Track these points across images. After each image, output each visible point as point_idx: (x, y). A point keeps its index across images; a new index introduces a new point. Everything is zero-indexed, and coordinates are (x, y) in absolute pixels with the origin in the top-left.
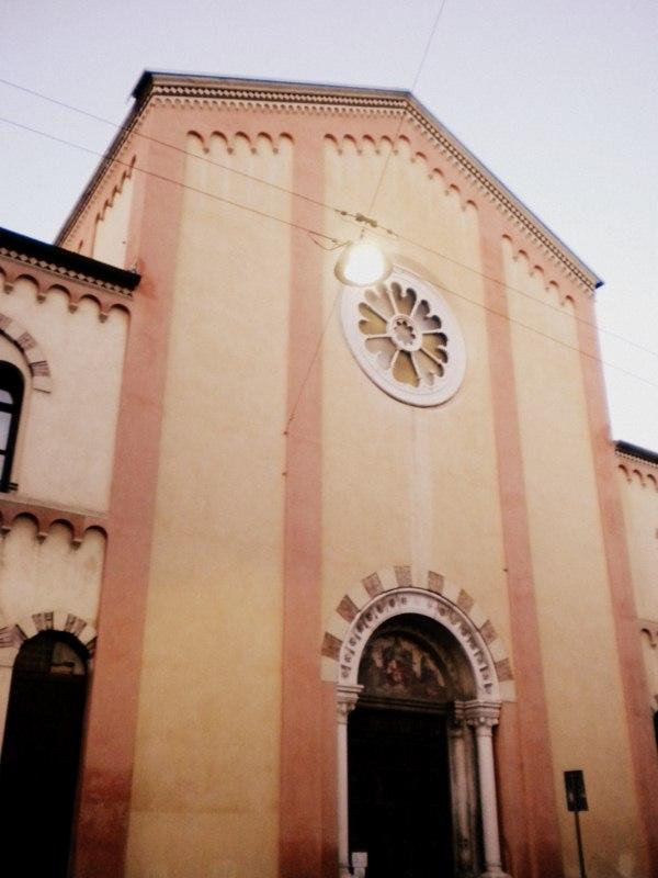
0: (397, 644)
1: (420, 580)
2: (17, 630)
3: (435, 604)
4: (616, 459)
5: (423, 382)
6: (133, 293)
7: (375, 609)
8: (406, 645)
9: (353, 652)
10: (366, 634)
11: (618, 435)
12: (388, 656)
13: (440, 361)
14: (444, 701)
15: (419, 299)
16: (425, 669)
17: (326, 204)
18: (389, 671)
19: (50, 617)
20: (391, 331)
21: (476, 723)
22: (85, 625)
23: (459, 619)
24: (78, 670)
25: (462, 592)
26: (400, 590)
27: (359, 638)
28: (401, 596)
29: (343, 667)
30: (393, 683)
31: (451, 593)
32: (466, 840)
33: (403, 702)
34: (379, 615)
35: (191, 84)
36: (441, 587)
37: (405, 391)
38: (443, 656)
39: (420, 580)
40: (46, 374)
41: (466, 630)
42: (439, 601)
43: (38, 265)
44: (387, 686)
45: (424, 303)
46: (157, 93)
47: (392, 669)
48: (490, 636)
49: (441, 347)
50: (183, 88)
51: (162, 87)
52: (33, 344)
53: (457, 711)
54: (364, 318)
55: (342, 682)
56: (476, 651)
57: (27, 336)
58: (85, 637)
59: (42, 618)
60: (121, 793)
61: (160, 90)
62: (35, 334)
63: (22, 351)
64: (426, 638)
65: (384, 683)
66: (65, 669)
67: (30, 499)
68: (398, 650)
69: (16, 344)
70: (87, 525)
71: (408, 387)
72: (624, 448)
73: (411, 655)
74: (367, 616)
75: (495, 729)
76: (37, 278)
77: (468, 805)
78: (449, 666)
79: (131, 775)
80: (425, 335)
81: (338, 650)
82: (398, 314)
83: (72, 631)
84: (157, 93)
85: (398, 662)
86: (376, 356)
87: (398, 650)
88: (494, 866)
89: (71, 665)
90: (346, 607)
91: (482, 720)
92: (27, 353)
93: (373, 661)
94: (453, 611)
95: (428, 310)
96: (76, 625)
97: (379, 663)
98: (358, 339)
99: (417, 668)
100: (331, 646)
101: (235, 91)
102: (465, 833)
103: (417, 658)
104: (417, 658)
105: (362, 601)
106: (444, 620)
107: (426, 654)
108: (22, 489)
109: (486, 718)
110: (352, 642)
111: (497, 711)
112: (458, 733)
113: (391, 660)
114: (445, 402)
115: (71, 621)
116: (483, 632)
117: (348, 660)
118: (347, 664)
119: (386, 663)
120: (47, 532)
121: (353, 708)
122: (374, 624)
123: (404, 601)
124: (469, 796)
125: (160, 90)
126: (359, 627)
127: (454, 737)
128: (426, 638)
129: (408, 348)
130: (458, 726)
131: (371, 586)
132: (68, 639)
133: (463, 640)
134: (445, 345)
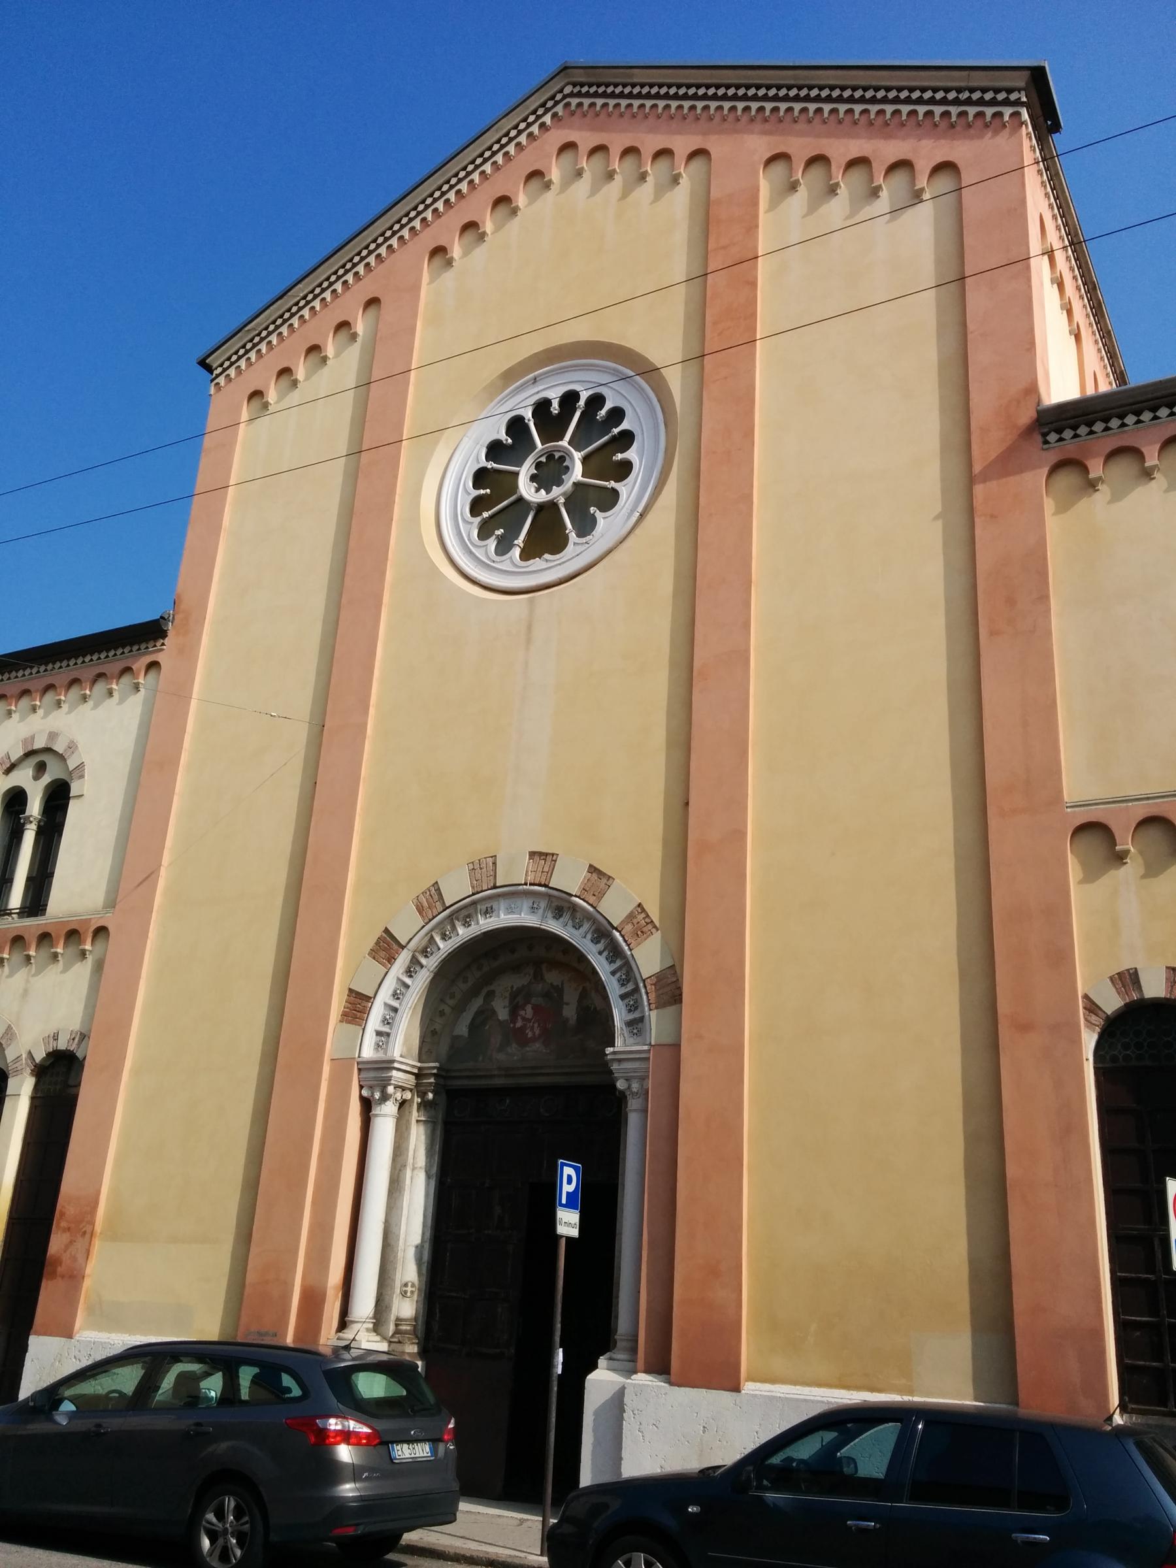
0: (538, 976)
7: (435, 1120)
8: (553, 977)
18: (519, 1024)
30: (523, 1042)
34: (482, 921)
44: (513, 1048)
47: (524, 1019)
68: (539, 987)
73: (560, 990)
76: (1127, 444)
85: (536, 1009)
87: (539, 987)
88: (635, 1110)
91: (390, 1089)
93: (494, 1012)
97: (503, 1014)
119: (514, 1011)
120: (618, 480)
121: (526, 421)
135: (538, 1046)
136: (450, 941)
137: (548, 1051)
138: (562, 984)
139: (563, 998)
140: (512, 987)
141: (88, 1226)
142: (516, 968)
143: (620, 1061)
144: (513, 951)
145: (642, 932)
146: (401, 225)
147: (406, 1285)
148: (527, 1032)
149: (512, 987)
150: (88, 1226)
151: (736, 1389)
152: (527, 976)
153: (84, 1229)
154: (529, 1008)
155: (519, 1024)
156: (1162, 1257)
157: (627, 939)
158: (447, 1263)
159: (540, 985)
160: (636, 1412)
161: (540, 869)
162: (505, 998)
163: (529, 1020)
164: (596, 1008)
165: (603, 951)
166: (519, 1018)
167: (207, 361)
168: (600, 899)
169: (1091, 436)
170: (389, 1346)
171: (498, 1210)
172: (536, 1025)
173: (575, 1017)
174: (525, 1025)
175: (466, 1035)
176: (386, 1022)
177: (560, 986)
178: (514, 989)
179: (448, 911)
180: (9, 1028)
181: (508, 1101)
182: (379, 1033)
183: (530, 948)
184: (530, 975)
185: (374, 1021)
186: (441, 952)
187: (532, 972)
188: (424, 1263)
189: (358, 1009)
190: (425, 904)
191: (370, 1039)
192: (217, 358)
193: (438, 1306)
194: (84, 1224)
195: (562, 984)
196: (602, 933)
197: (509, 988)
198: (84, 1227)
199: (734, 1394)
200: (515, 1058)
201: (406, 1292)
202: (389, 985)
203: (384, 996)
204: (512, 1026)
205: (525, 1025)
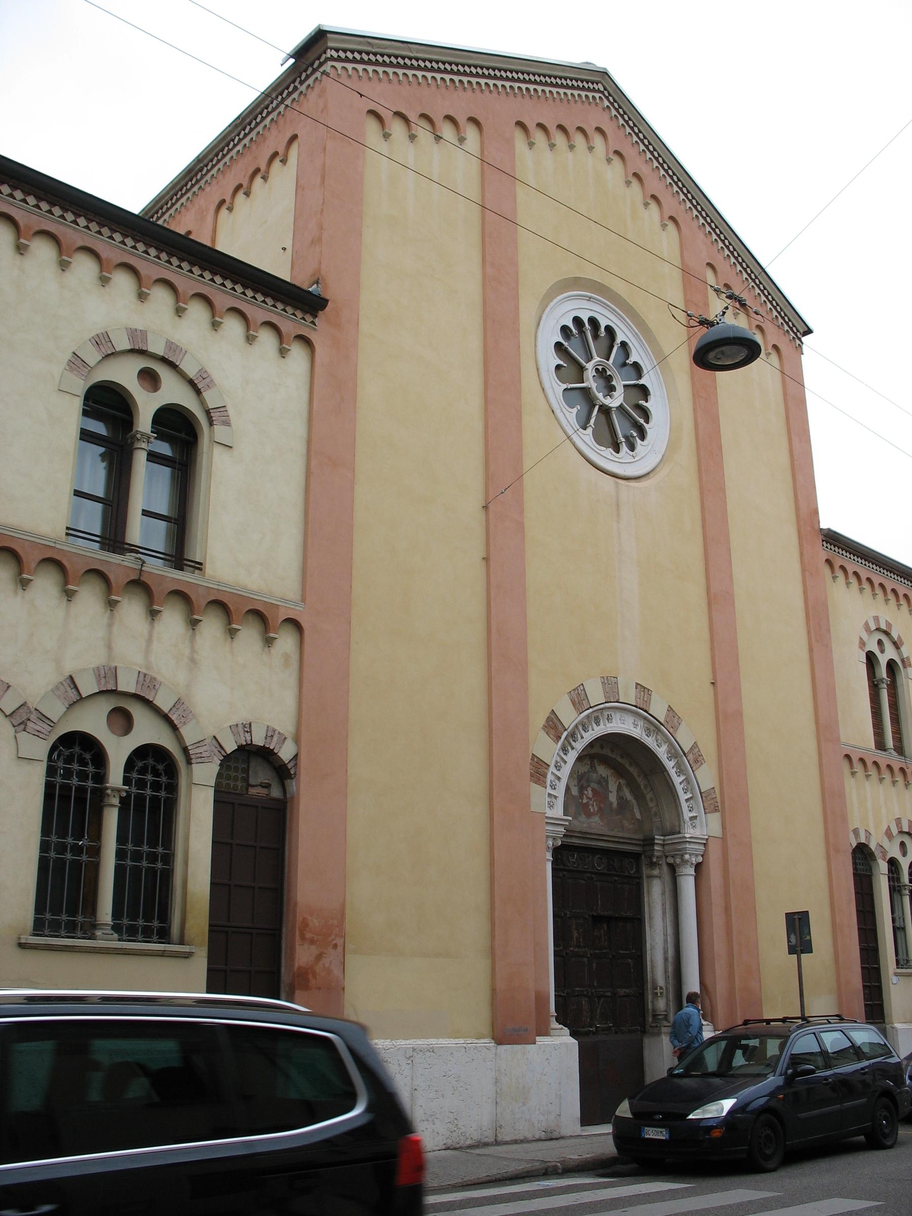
0: (593, 768)
1: (629, 695)
2: (214, 742)
3: (641, 723)
4: (822, 553)
5: (624, 448)
6: (316, 321)
7: (580, 728)
8: (603, 771)
9: (559, 779)
10: (572, 757)
11: (825, 523)
12: (584, 782)
13: (642, 421)
14: (639, 836)
16: (620, 798)
18: (585, 801)
19: (248, 728)
20: (591, 381)
21: (678, 861)
22: (285, 738)
23: (667, 740)
24: (276, 793)
25: (670, 709)
26: (607, 705)
27: (565, 762)
28: (606, 713)
29: (550, 795)
30: (589, 815)
31: (658, 710)
33: (599, 837)
34: (585, 735)
35: (369, 49)
36: (648, 702)
37: (604, 456)
38: (641, 781)
39: (629, 695)
40: (227, 423)
41: (673, 754)
42: (645, 718)
43: (212, 280)
44: (583, 818)
45: (624, 345)
46: (332, 59)
47: (588, 798)
48: (696, 761)
49: (642, 402)
50: (360, 52)
51: (337, 50)
52: (211, 385)
53: (656, 848)
54: (561, 363)
55: (550, 813)
56: (682, 778)
57: (203, 373)
58: (286, 753)
59: (240, 728)
60: (296, 904)
61: (335, 54)
62: (215, 374)
63: (198, 392)
64: (625, 762)
66: (263, 791)
67: (219, 583)
69: (192, 383)
70: (282, 617)
71: (609, 452)
72: (833, 539)
73: (607, 782)
74: (573, 735)
75: (698, 867)
77: (665, 952)
78: (649, 796)
79: (343, 914)
80: (625, 386)
81: (545, 776)
82: (597, 359)
83: (271, 748)
84: (332, 59)
86: (575, 410)
89: (267, 786)
90: (553, 725)
91: (687, 857)
92: (206, 395)
94: (659, 730)
95: (627, 356)
96: (275, 738)
98: (556, 388)
99: (613, 798)
100: (539, 771)
101: (417, 59)
102: (661, 982)
103: (613, 786)
104: (613, 786)
105: (569, 717)
106: (650, 741)
107: (623, 782)
108: (209, 569)
110: (558, 768)
112: (656, 872)
113: (586, 789)
114: (648, 473)
115: (271, 733)
116: (691, 757)
117: (553, 787)
118: (552, 792)
122: (580, 745)
123: (609, 719)
124: (666, 941)
126: (564, 750)
127: (650, 877)
128: (625, 762)
129: (608, 401)
130: (652, 865)
131: (579, 698)
132: (266, 754)
133: (669, 765)
134: (647, 402)
140: (578, 772)
141: (337, 938)
149: (578, 772)
150: (337, 938)
153: (334, 942)
154: (589, 789)
155: (585, 801)
162: (574, 779)
163: (591, 799)
167: (328, 35)
168: (676, 731)
169: (85, 230)
172: (595, 804)
174: (588, 802)
179: (591, 710)
180: (25, 702)
181: (576, 856)
187: (589, 763)
190: (576, 700)
192: (336, 41)
194: (333, 937)
197: (576, 772)
198: (333, 940)
205: (588, 802)
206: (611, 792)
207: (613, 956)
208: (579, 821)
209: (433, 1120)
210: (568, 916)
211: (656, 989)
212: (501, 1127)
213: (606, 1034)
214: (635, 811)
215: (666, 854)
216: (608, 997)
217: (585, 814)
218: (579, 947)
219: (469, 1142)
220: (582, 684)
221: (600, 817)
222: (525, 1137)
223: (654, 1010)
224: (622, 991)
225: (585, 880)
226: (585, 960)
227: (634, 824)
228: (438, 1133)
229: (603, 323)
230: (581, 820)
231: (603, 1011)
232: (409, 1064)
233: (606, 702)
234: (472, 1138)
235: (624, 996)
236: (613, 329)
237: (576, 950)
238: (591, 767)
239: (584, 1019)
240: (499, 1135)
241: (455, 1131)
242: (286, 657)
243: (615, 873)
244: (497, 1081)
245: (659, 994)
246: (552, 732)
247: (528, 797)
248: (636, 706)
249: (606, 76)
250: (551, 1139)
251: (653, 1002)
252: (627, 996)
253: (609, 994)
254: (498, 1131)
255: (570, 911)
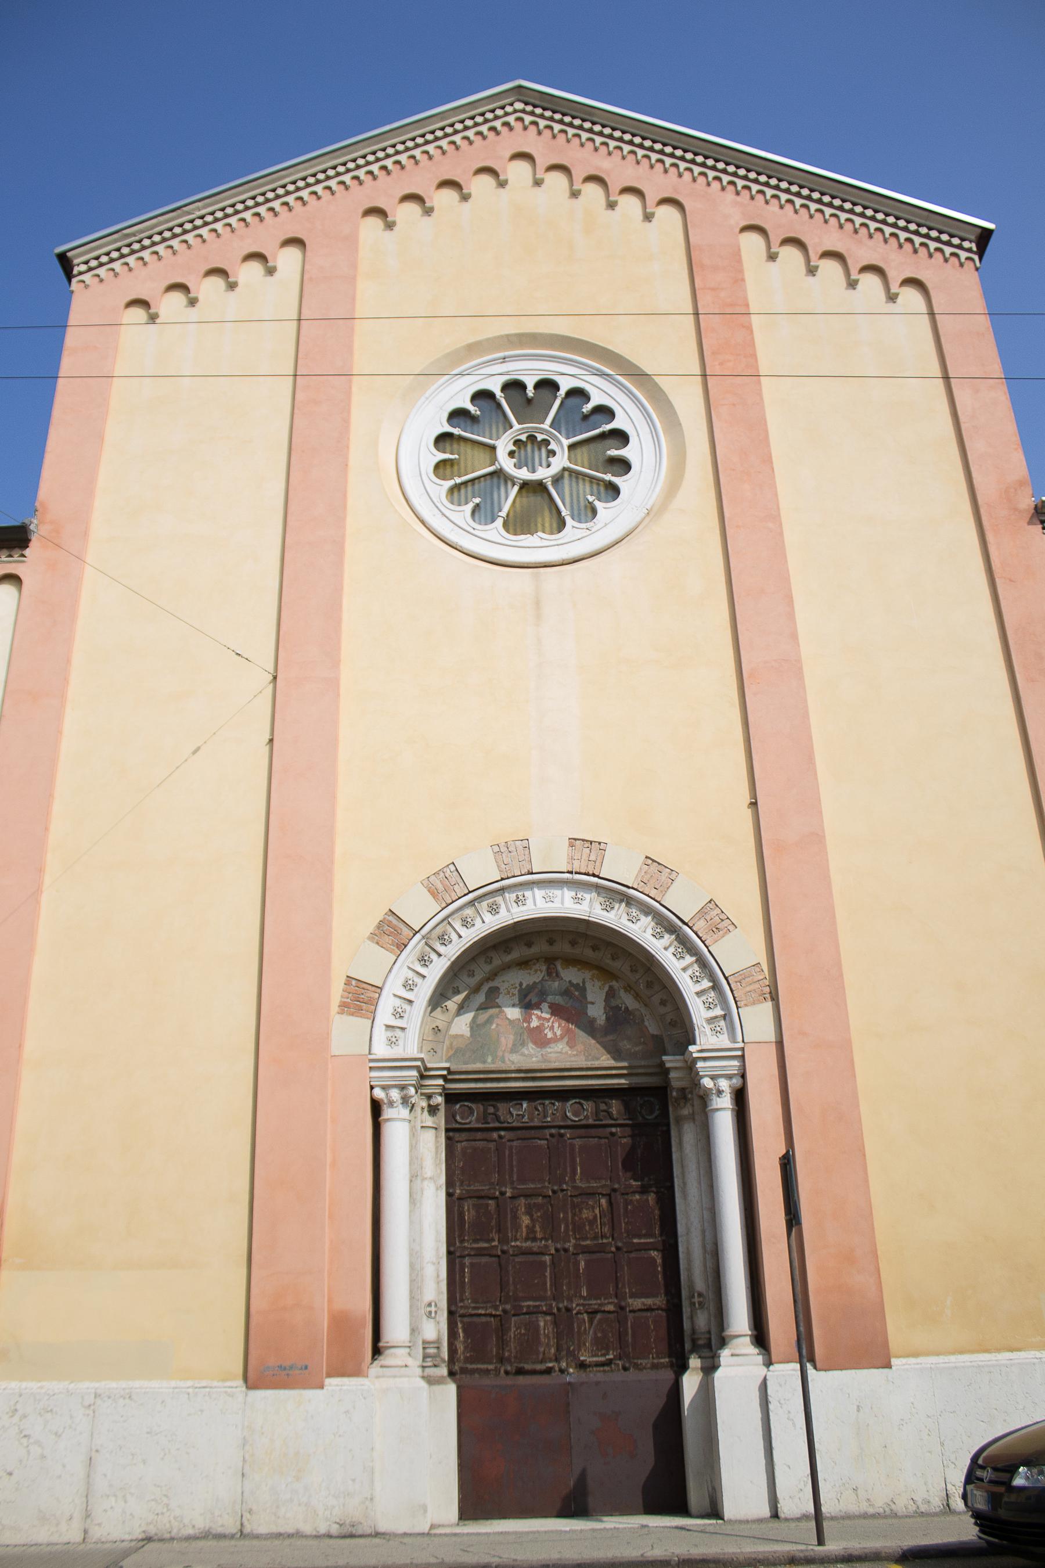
8: (571, 975)
15: (496, 388)
17: (988, 316)
32: (700, 1295)
33: (562, 1072)
41: (668, 925)
42: (597, 887)
44: (531, 1048)
46: (81, 273)
61: (83, 268)
65: (523, 1044)
73: (583, 989)
81: (374, 1003)
102: (700, 1285)
109: (713, 1078)
111: (736, 1063)
112: (685, 1112)
122: (453, 951)
125: (83, 268)
135: (561, 1047)
136: (472, 929)
137: (575, 1053)
138: (584, 982)
139: (586, 998)
140: (521, 984)
142: (524, 964)
143: (705, 1059)
144: (529, 945)
145: (717, 928)
146: (896, 223)
147: (430, 1305)
148: (545, 1032)
149: (521, 984)
151: (889, 1366)
152: (539, 972)
156: (573, 1324)
157: (701, 936)
158: (466, 1280)
159: (556, 984)
160: (782, 1401)
161: (585, 857)
162: (514, 995)
164: (627, 1008)
165: (670, 946)
166: (533, 1017)
170: (423, 1371)
171: (526, 1221)
172: (556, 1025)
173: (604, 1017)
175: (468, 1034)
176: (398, 1015)
177: (581, 985)
178: (524, 986)
182: (388, 1027)
183: (551, 942)
184: (541, 972)
185: (384, 1014)
186: (464, 941)
187: (544, 968)
188: (443, 1280)
189: (361, 1000)
190: (440, 887)
191: (380, 1035)
193: (460, 1325)
195: (584, 982)
196: (668, 925)
197: (517, 985)
199: (886, 1370)
200: (534, 1059)
201: (430, 1312)
202: (401, 973)
203: (394, 986)
204: (525, 1025)
206: (593, 1003)
207: (618, 1249)
208: (523, 1055)
209: (124, 1496)
210: (508, 1194)
211: (693, 1296)
212: (250, 1511)
213: (604, 1371)
214: (646, 1023)
215: (372, 1083)
216: (609, 1312)
217: (535, 1043)
218: (534, 1239)
219: (190, 1531)
220: (453, 863)
221: (567, 1043)
222: (297, 1530)
223: (694, 1331)
224: (637, 1303)
225: (547, 1139)
226: (547, 1258)
227: (644, 1043)
228: (131, 1514)
229: (495, 386)
230: (526, 1052)
231: (599, 1335)
232: (88, 1415)
233: (502, 879)
234: (194, 1526)
235: (640, 1310)
236: (519, 380)
237: (528, 1244)
238: (549, 974)
239: (542, 1349)
240: (246, 1523)
241: (162, 1514)
242: (722, 925)
243: (613, 1122)
244: (245, 1442)
245: (697, 1305)
246: (387, 939)
247: (326, 1037)
248: (571, 873)
249: (524, 90)
250: (352, 1536)
251: (692, 1318)
252: (649, 1309)
253: (611, 1308)
254: (244, 1518)
255: (513, 1188)
